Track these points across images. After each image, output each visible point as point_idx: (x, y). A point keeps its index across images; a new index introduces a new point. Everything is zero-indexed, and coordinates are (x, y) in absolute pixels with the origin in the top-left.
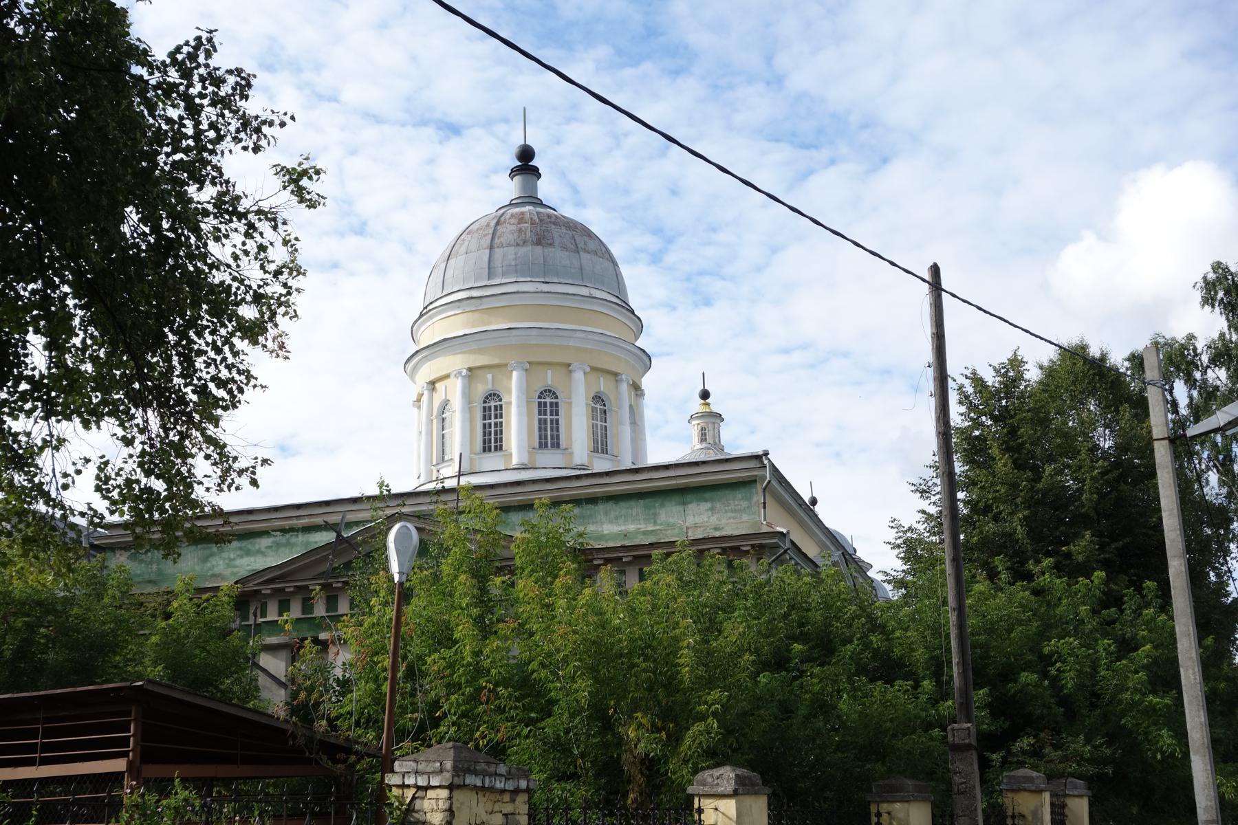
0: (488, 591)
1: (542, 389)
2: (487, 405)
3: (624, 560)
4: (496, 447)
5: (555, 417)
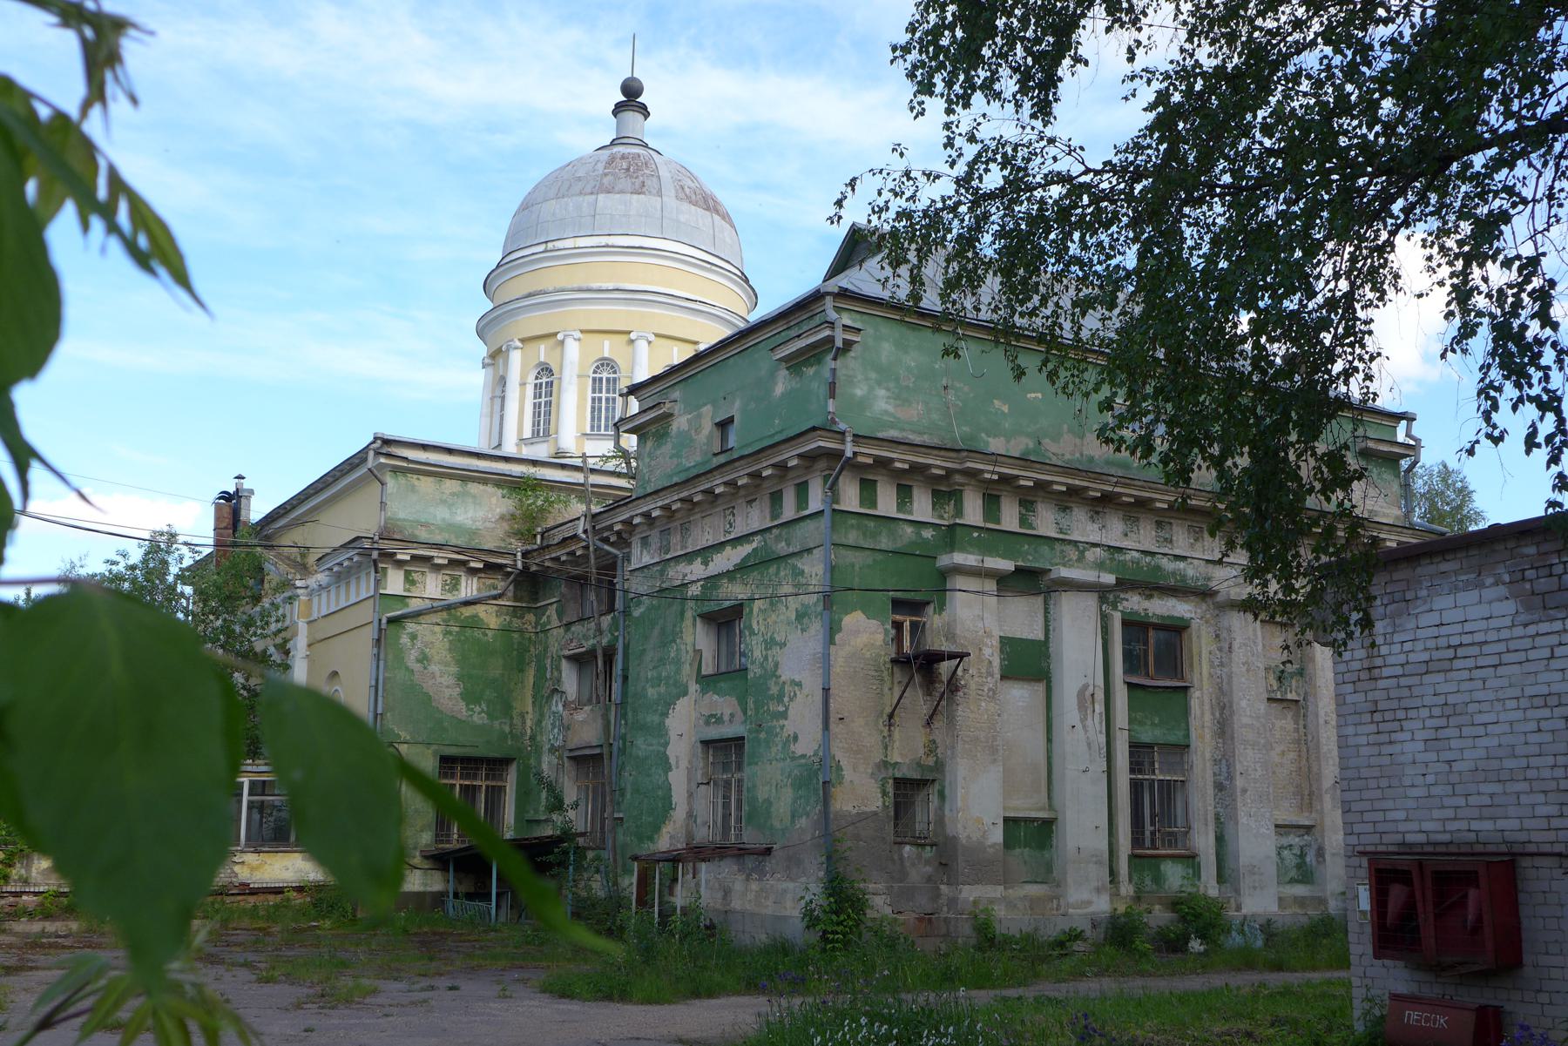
5: (597, 395)
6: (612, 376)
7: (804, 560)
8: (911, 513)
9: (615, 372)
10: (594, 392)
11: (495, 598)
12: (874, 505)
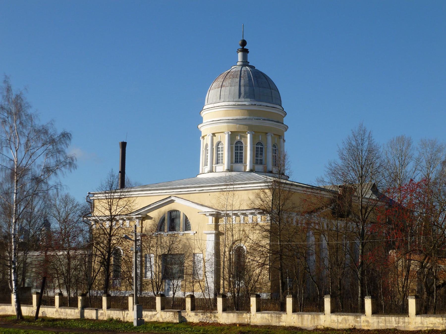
0: (174, 218)
3: (255, 213)
4: (240, 161)
5: (237, 151)
6: (261, 147)
10: (236, 150)
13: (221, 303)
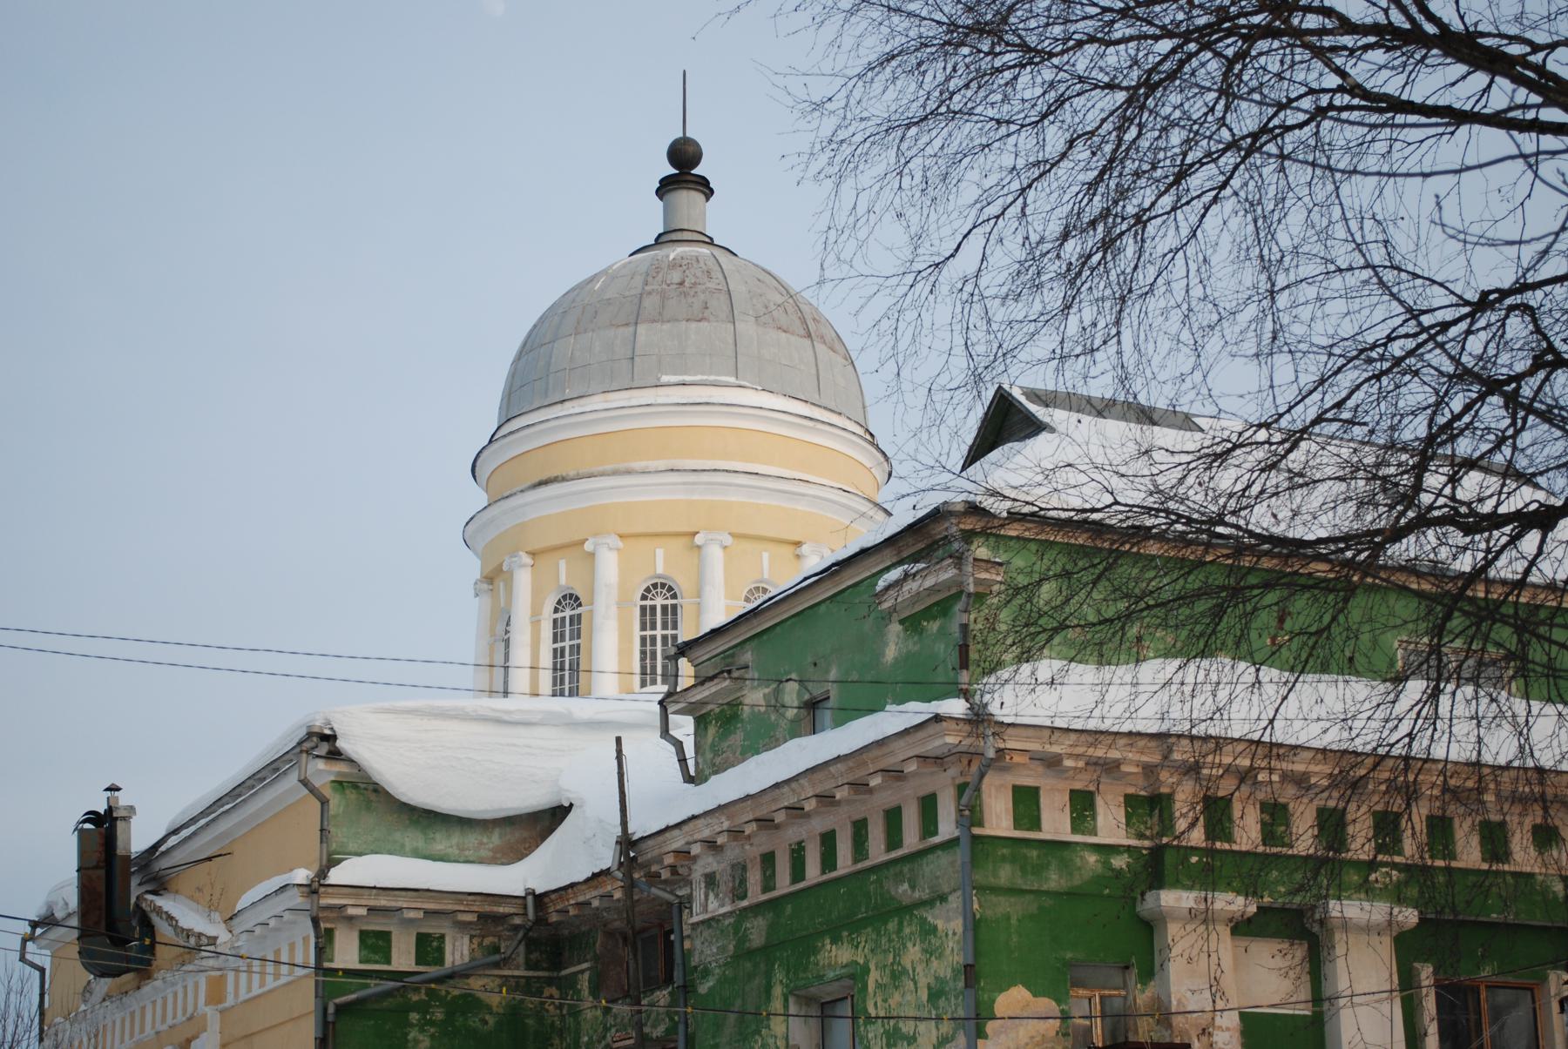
1: (649, 583)
2: (648, 603)
5: (649, 633)
6: (670, 602)
7: (936, 911)
8: (1094, 833)
9: (674, 596)
10: (643, 628)
11: (496, 965)
12: (1036, 824)
13: (1025, 784)
